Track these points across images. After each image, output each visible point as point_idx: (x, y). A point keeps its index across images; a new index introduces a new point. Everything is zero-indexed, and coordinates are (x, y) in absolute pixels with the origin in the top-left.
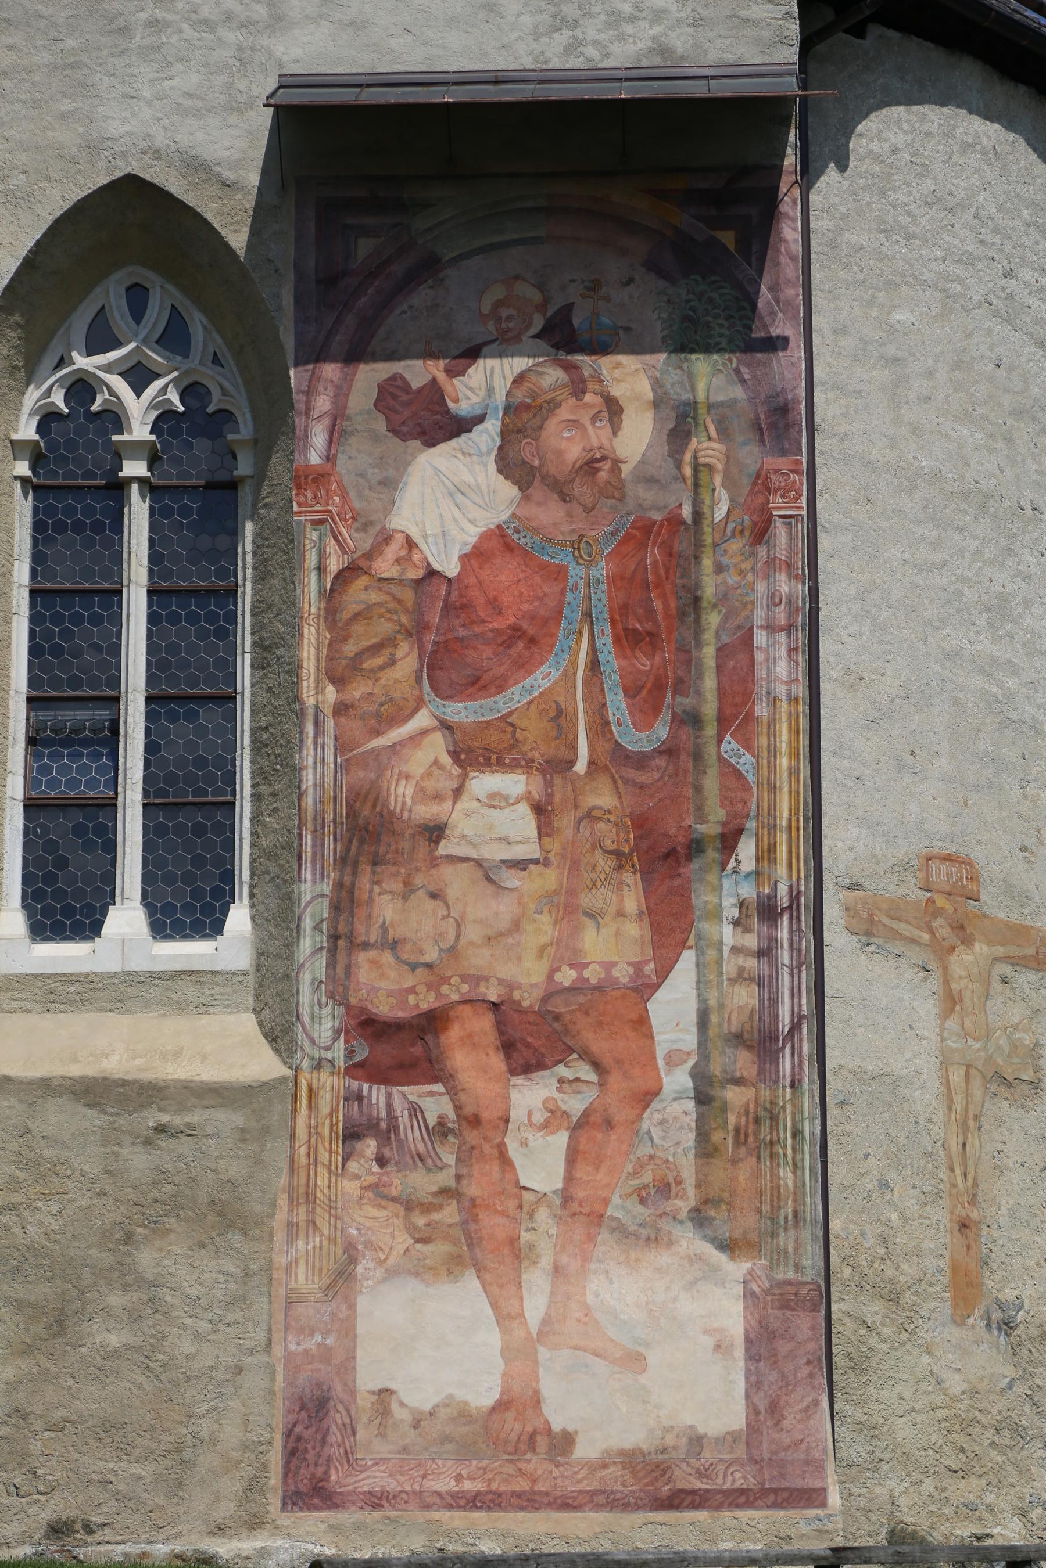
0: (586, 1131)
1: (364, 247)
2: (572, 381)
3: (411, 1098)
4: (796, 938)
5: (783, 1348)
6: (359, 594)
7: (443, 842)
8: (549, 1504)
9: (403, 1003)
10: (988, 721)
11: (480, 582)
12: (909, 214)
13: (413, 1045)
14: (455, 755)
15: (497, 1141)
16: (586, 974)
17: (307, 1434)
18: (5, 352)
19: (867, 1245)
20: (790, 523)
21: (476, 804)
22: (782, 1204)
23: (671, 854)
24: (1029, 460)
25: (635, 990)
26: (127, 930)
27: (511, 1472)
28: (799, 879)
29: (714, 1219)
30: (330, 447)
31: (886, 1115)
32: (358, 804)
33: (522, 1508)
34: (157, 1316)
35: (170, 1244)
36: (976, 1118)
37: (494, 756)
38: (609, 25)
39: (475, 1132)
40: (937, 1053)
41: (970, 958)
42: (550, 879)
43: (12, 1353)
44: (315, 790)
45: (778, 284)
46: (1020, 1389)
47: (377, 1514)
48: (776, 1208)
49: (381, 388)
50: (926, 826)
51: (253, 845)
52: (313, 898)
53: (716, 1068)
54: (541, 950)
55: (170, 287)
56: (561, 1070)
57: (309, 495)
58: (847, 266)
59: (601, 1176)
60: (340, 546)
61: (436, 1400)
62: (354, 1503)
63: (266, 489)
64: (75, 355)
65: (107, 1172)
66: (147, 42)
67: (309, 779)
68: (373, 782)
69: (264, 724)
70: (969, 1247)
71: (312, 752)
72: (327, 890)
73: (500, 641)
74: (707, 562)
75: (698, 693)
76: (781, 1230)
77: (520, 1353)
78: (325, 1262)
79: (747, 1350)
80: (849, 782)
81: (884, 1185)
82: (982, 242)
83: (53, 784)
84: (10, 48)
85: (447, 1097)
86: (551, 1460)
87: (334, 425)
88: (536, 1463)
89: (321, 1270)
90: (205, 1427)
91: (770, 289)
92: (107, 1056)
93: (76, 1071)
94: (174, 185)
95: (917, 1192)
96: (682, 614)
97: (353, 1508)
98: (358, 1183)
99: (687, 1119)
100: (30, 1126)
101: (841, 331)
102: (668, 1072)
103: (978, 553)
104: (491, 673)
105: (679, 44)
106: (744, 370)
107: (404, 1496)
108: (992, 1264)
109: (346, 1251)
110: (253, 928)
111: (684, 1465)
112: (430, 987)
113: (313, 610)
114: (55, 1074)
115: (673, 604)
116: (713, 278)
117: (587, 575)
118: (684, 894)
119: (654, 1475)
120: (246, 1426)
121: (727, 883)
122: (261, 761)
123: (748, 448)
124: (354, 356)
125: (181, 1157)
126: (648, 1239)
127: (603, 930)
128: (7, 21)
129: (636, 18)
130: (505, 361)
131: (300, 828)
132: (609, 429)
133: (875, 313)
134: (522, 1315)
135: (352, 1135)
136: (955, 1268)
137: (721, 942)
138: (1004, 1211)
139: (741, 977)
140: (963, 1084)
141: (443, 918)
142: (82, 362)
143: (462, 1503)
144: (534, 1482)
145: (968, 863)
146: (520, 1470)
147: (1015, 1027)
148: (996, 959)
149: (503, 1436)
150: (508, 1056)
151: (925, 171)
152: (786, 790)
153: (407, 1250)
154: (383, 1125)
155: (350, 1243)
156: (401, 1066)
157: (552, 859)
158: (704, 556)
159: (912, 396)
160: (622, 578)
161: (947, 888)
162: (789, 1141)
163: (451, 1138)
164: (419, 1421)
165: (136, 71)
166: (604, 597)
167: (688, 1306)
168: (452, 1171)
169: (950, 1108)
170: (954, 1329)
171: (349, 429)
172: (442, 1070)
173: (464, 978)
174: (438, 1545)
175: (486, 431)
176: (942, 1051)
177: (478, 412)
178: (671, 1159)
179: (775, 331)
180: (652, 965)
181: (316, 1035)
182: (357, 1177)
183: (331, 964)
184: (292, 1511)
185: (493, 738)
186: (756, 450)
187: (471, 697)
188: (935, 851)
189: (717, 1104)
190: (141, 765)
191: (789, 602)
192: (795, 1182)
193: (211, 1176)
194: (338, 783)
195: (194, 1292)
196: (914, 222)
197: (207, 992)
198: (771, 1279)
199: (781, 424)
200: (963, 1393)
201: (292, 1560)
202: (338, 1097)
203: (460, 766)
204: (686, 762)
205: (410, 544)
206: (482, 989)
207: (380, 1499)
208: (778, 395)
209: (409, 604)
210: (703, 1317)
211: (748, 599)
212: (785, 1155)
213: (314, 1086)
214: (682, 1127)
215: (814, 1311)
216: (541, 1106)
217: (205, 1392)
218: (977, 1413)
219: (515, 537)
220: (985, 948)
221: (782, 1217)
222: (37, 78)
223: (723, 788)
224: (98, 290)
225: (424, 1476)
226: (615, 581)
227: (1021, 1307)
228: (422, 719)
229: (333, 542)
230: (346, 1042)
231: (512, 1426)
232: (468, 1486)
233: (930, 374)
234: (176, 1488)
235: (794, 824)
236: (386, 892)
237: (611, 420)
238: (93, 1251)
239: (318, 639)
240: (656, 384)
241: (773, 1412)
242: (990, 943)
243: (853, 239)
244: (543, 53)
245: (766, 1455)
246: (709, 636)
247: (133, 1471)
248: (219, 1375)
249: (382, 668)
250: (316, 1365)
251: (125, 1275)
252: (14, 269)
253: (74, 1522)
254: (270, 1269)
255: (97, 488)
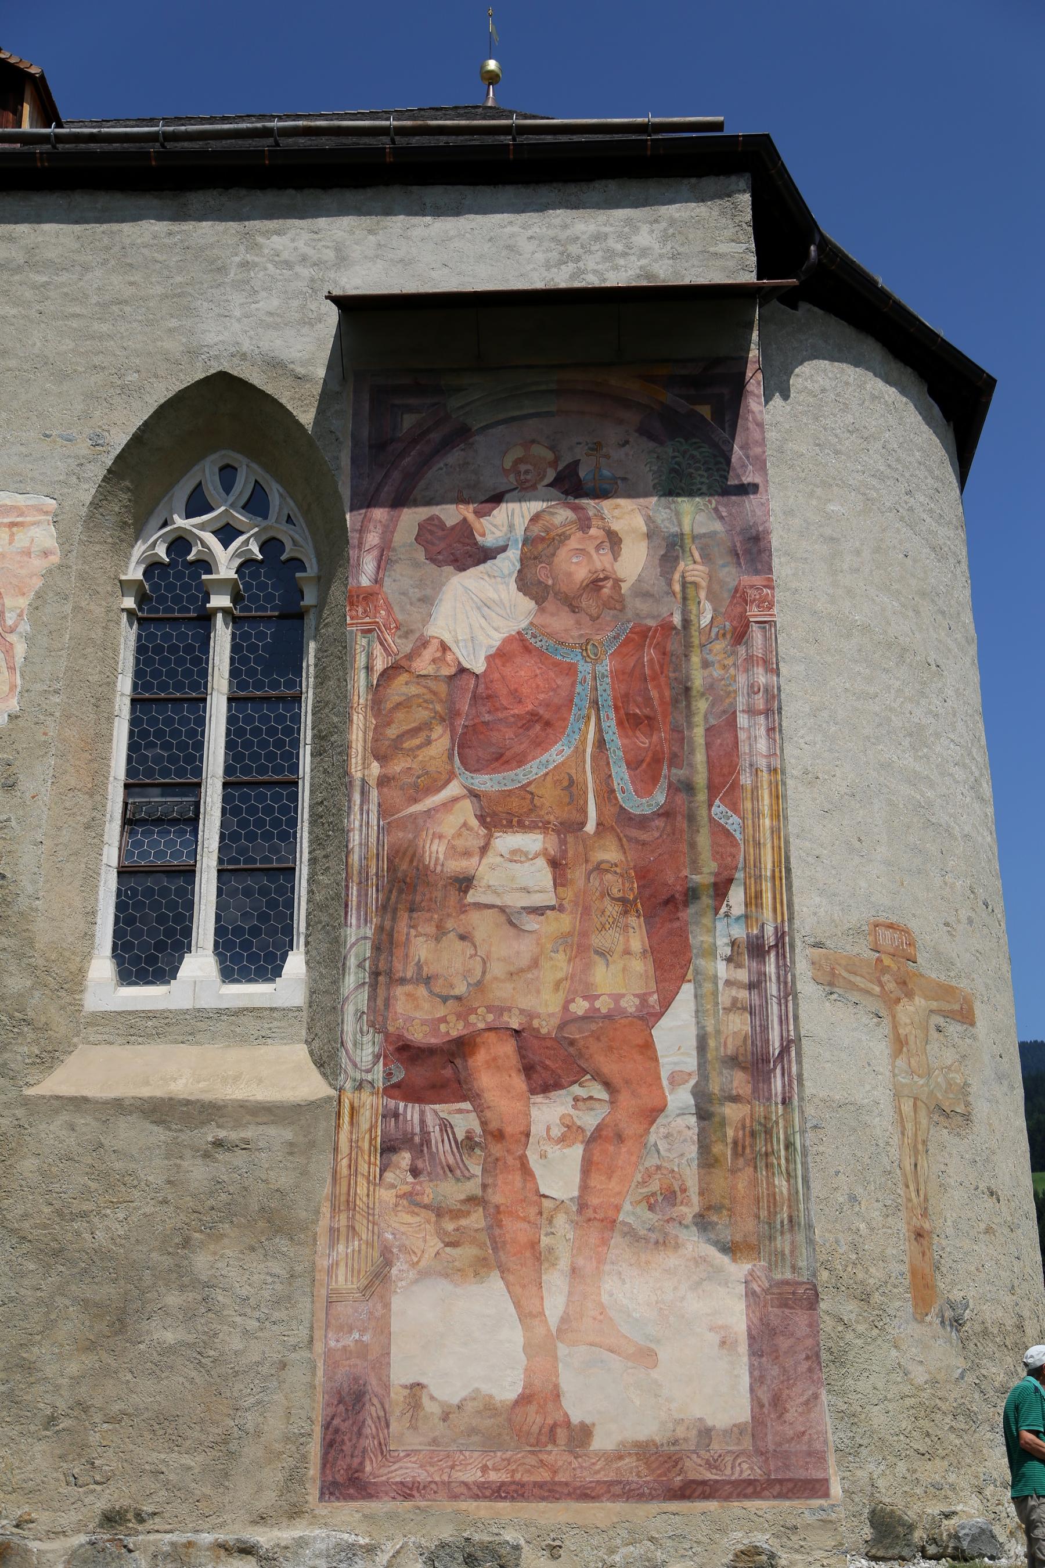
0: (599, 1144)
1: (408, 421)
2: (579, 519)
3: (442, 1115)
4: (782, 973)
5: (784, 1343)
6: (401, 688)
7: (471, 892)
8: (569, 1495)
9: (435, 1031)
10: (915, 820)
11: (503, 677)
12: (836, 436)
13: (444, 1068)
14: (481, 818)
15: (520, 1153)
16: (597, 1004)
17: (344, 1427)
18: (117, 509)
19: (841, 1251)
20: (764, 628)
21: (499, 859)
22: (778, 1209)
23: (670, 901)
24: (931, 629)
25: (641, 1018)
26: (199, 973)
27: (533, 1463)
28: (783, 921)
29: (717, 1224)
30: (378, 573)
31: (852, 1138)
32: (397, 860)
33: (543, 1499)
34: (210, 1315)
35: (223, 1248)
36: (924, 1142)
37: (516, 819)
38: (605, 259)
39: (499, 1146)
40: (891, 1087)
41: (912, 1009)
42: (565, 922)
43: (78, 1350)
44: (361, 848)
45: (747, 444)
46: (970, 1378)
47: (408, 1504)
48: (772, 1214)
49: (421, 526)
50: (873, 899)
51: (309, 901)
52: (358, 940)
53: (715, 1087)
54: (557, 985)
55: (254, 466)
56: (576, 1090)
57: (360, 610)
58: (791, 467)
59: (614, 1185)
60: (385, 649)
61: (464, 1394)
62: (387, 1494)
63: (326, 612)
64: (176, 517)
65: (169, 1182)
66: (239, 277)
67: (355, 839)
68: (410, 841)
69: (319, 800)
70: (924, 1254)
71: (358, 817)
72: (369, 933)
73: (520, 725)
74: (695, 660)
75: (691, 765)
76: (778, 1234)
77: (541, 1350)
78: (363, 1265)
79: (750, 1346)
80: (810, 859)
81: (853, 1199)
82: (889, 466)
83: (143, 855)
84: (131, 284)
85: (474, 1114)
86: (571, 1452)
87: (382, 555)
88: (556, 1455)
89: (359, 1272)
90: (251, 1420)
91: (741, 448)
92: (175, 1080)
93: (146, 1092)
94: (256, 378)
95: (880, 1205)
96: (675, 701)
97: (386, 1498)
98: (394, 1191)
99: (690, 1133)
100: (103, 1141)
101: (789, 513)
102: (672, 1091)
103: (899, 690)
104: (512, 751)
105: (661, 272)
106: (721, 509)
107: (433, 1486)
108: (943, 1269)
109: (382, 1254)
110: (307, 971)
111: (694, 1456)
112: (459, 1016)
113: (362, 701)
114: (126, 1095)
115: (667, 693)
116: (694, 440)
117: (594, 670)
118: (682, 935)
119: (667, 1465)
120: (288, 1419)
121: (720, 925)
122: (316, 830)
123: (726, 569)
124: (399, 501)
125: (236, 1169)
126: (657, 1242)
127: (611, 967)
128: (131, 265)
129: (626, 254)
130: (523, 504)
131: (347, 880)
132: (610, 556)
133: (814, 502)
134: (542, 1313)
135: (389, 1148)
136: (914, 1272)
137: (716, 977)
138: (949, 1223)
139: (735, 1006)
140: (912, 1114)
141: (471, 956)
142: (180, 522)
143: (488, 1493)
144: (555, 1472)
145: (906, 931)
146: (541, 1461)
147: (949, 1068)
148: (931, 1011)
149: (525, 1428)
150: (528, 1077)
151: (846, 408)
152: (769, 845)
153: (438, 1253)
154: (417, 1139)
155: (386, 1247)
156: (433, 1087)
157: (566, 905)
158: (693, 654)
159: (845, 567)
160: (624, 673)
161: (892, 951)
162: (783, 1153)
163: (478, 1151)
164: (448, 1414)
165: (230, 298)
166: (608, 688)
167: (695, 1305)
168: (479, 1181)
169: (903, 1134)
170: (916, 1325)
171: (394, 558)
172: (470, 1090)
173: (490, 1009)
174: (465, 1535)
175: (508, 558)
176: (894, 1085)
177: (501, 543)
178: (676, 1169)
179: (746, 480)
180: (655, 996)
181: (358, 1060)
182: (393, 1186)
183: (373, 998)
184: (329, 1501)
185: (515, 804)
186: (734, 570)
187: (495, 771)
188: (881, 920)
189: (717, 1119)
190: (216, 838)
191: (766, 690)
192: (789, 1190)
193: (262, 1186)
194: (381, 842)
195: (244, 1292)
196: (840, 442)
197: (266, 1026)
198: (770, 1279)
199: (755, 550)
200: (926, 1383)
201: (328, 1550)
202: (377, 1115)
203: (486, 828)
204: (682, 823)
205: (444, 647)
206: (506, 1018)
207: (411, 1489)
208: (751, 527)
209: (443, 696)
210: (709, 1315)
211: (731, 688)
212: (779, 1165)
213: (356, 1104)
214: (685, 1140)
215: (810, 1309)
216: (558, 1121)
217: (251, 1386)
218: (938, 1401)
219: (533, 641)
220: (923, 1001)
221: (778, 1222)
222: (151, 304)
223: (714, 844)
224: (196, 468)
225: (452, 1467)
226: (617, 675)
227: (967, 1307)
228: (453, 789)
229: (379, 647)
230: (385, 1065)
231: (534, 1419)
232: (493, 1476)
233: (858, 553)
234: (223, 1477)
235: (777, 874)
236: (421, 935)
237: (612, 549)
238: (154, 1255)
239: (365, 725)
240: (649, 520)
241: (776, 1405)
242: (926, 998)
243: (796, 448)
244: (553, 279)
245: (771, 1447)
246: (699, 719)
247: (183, 1461)
248: (264, 1370)
249: (419, 747)
250: (353, 1361)
251: (181, 1276)
252: (125, 442)
253: (127, 1511)
254: (313, 1271)
255: (190, 619)
